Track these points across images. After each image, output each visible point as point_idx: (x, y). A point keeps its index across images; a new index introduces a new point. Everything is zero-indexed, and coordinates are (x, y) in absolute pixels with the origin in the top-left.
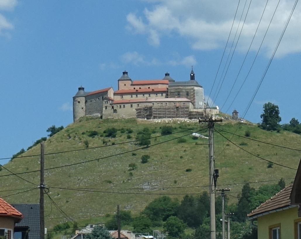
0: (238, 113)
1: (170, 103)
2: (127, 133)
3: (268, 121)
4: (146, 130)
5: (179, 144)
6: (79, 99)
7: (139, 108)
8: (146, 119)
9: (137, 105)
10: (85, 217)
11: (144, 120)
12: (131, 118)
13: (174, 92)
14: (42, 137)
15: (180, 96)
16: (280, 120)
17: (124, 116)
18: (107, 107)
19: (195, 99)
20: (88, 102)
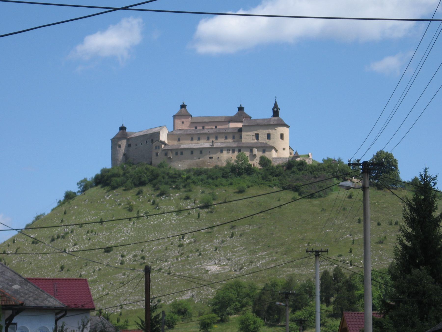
10: (142, 279)
14: (66, 190)
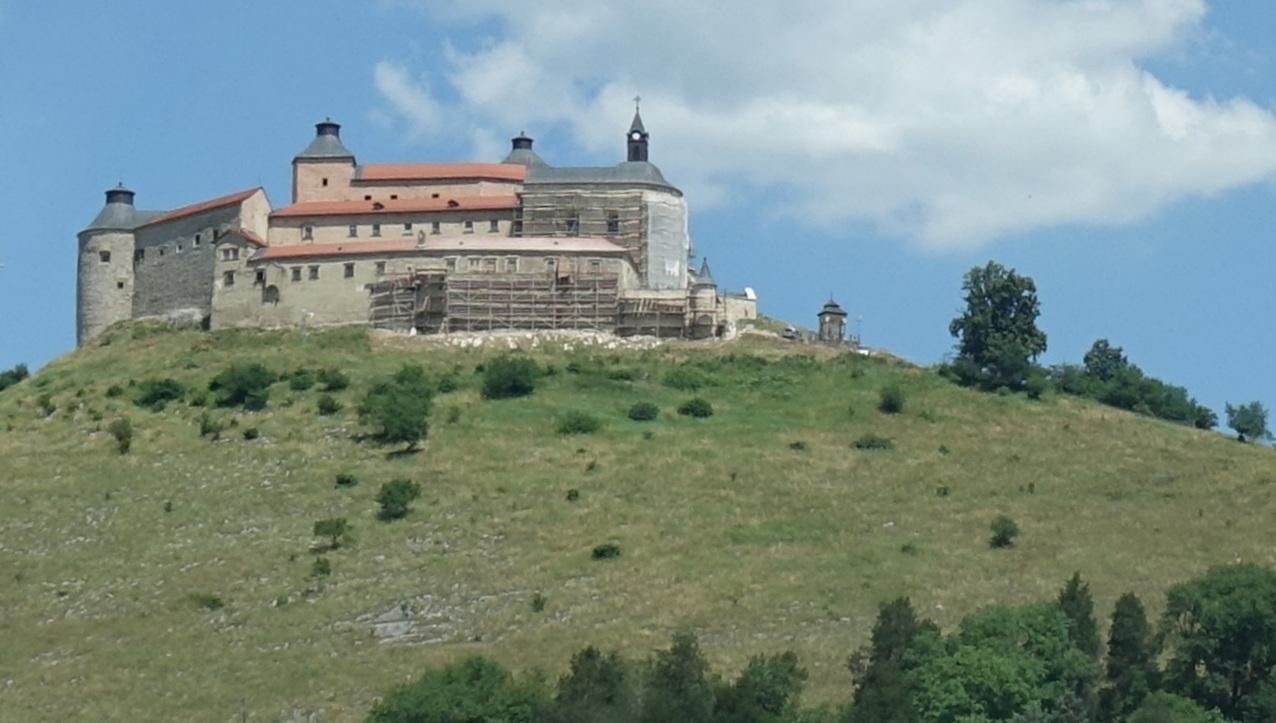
0: (845, 315)
1: (528, 258)
2: (319, 390)
3: (987, 346)
4: (410, 376)
5: (564, 441)
6: (104, 243)
7: (382, 279)
8: (414, 331)
9: (375, 267)
11: (405, 338)
12: (343, 327)
13: (550, 215)
15: (577, 230)
16: (1042, 346)
17: (312, 314)
18: (235, 275)
19: (649, 248)
20: (146, 254)
